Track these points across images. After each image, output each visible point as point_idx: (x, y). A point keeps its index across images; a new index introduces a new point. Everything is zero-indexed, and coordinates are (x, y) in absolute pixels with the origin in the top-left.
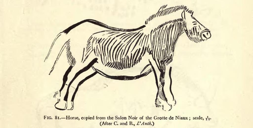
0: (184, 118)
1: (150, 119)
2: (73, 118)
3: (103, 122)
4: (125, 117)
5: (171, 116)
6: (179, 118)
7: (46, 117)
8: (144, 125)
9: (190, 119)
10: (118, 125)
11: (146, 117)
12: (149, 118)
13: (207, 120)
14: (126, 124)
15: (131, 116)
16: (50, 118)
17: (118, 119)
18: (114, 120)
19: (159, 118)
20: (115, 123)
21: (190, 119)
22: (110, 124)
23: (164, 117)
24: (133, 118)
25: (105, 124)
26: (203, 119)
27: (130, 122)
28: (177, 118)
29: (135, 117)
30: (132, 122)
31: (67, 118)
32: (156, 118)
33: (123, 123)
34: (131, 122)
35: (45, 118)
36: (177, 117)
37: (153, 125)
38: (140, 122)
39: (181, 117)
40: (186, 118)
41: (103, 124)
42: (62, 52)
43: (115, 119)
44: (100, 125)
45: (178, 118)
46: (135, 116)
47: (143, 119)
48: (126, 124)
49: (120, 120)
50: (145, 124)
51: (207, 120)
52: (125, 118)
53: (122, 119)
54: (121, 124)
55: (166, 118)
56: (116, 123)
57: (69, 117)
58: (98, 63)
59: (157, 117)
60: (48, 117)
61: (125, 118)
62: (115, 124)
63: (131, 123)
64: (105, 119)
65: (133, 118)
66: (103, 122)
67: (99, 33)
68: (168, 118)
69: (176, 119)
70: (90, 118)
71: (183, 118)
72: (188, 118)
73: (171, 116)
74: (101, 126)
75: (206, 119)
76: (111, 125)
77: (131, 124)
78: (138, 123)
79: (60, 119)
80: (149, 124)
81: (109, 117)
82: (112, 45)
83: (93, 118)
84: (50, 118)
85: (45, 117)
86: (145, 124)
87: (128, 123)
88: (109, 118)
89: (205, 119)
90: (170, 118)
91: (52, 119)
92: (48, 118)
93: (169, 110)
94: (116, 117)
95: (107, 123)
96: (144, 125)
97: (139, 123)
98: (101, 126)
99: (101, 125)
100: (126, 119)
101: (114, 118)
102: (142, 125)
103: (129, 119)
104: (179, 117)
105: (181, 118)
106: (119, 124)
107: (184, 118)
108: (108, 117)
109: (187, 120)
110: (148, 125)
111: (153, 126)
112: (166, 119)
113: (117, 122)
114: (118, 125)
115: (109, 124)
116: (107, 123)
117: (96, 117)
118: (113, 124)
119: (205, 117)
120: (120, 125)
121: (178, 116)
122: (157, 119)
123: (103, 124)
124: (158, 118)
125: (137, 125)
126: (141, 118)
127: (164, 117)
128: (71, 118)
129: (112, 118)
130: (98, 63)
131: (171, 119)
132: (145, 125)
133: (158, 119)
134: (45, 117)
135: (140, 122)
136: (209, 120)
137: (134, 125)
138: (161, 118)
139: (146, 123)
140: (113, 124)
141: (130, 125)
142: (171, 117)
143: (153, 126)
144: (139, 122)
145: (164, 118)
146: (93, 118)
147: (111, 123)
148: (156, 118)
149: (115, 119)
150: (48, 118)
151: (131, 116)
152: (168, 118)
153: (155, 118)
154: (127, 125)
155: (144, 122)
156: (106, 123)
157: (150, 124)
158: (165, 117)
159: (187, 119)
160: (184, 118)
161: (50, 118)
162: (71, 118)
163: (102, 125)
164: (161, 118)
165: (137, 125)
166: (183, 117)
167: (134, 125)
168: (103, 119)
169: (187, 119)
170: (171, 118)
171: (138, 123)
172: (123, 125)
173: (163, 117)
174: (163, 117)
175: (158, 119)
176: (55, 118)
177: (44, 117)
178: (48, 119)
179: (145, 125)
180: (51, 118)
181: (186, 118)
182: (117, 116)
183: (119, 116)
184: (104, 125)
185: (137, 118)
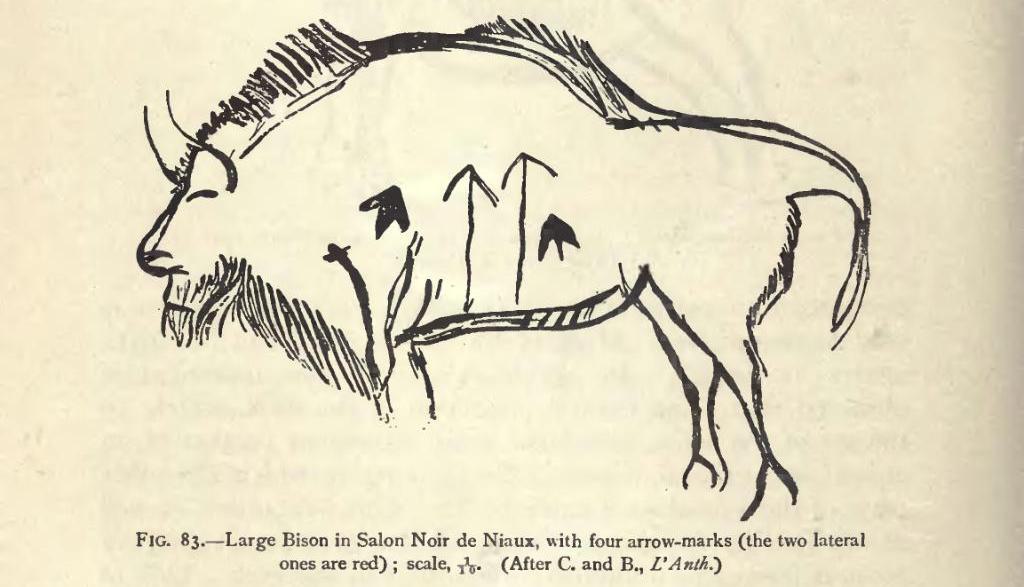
0: (519, 543)
2: (846, 539)
3: (516, 558)
4: (321, 539)
5: (465, 534)
6: (498, 542)
7: (144, 539)
9: (395, 569)
10: (573, 569)
12: (758, 541)
13: (355, 568)
14: (607, 566)
15: (424, 534)
16: (160, 541)
17: (370, 545)
18: (624, 550)
20: (564, 561)
21: (395, 569)
22: (544, 566)
24: (432, 542)
25: (523, 566)
26: (449, 569)
28: (417, 542)
29: (436, 537)
33: (595, 563)
34: (628, 561)
35: (142, 542)
36: (492, 540)
43: (359, 545)
45: (423, 543)
46: (439, 534)
48: (607, 566)
49: (706, 547)
50: (682, 566)
51: (355, 568)
52: (701, 543)
53: (429, 545)
54: (586, 566)
56: (565, 563)
58: (349, 247)
60: (152, 537)
62: (564, 567)
63: (627, 564)
64: (326, 545)
65: (432, 542)
66: (516, 558)
69: (414, 545)
70: (790, 542)
73: (465, 534)
75: (461, 567)
76: (547, 569)
77: (628, 567)
79: (203, 545)
82: (620, 277)
85: (142, 536)
86: (682, 566)
87: (617, 564)
89: (455, 570)
90: (462, 542)
91: (168, 545)
94: (363, 536)
95: (532, 562)
96: (678, 569)
97: (660, 563)
101: (355, 540)
102: (671, 569)
103: (486, 545)
104: (498, 537)
106: (579, 566)
107: (516, 542)
109: (529, 548)
110: (696, 569)
111: (716, 573)
114: (573, 569)
116: (529, 560)
117: (592, 539)
118: (554, 566)
121: (495, 534)
123: (514, 564)
125: (653, 569)
129: (765, 541)
130: (349, 247)
136: (472, 571)
137: (642, 570)
138: (656, 543)
139: (687, 564)
140: (554, 566)
141: (624, 569)
143: (716, 573)
145: (831, 542)
149: (359, 545)
151: (424, 534)
154: (611, 569)
156: (526, 562)
157: (703, 564)
160: (516, 542)
161: (160, 541)
163: (512, 569)
165: (653, 569)
172: (595, 569)
177: (139, 539)
178: (152, 545)
180: (164, 542)
181: (525, 542)
182: (366, 534)
183: (373, 534)
184: (520, 569)
185: (445, 540)
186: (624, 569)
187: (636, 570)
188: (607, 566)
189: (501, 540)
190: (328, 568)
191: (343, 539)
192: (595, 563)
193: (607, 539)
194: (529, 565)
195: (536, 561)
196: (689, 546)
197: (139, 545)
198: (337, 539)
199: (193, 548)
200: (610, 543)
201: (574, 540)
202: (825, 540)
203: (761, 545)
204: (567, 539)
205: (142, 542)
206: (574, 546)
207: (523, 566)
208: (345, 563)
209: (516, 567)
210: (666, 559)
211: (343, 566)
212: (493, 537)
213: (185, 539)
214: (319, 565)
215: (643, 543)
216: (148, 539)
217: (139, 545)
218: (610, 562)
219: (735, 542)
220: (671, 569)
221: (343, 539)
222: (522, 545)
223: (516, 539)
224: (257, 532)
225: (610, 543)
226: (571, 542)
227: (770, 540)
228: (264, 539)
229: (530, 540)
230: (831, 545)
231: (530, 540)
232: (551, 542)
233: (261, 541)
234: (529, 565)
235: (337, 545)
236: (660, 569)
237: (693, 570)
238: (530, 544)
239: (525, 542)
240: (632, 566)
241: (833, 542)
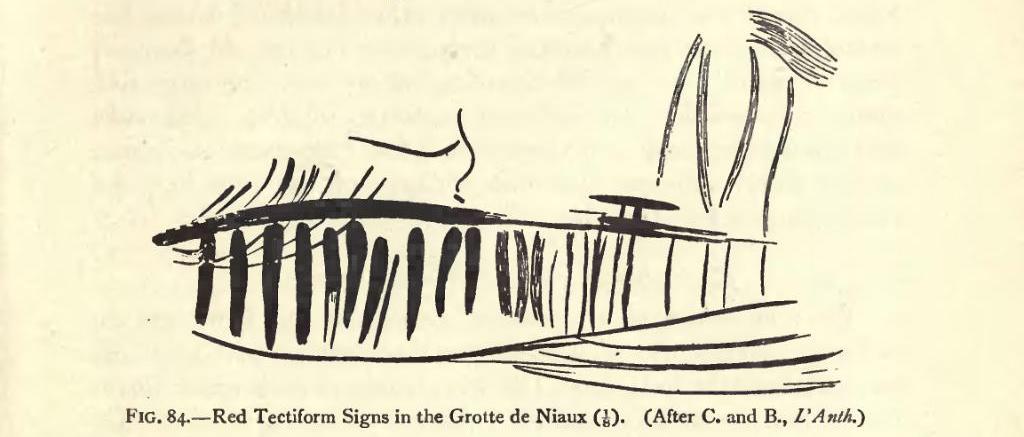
1: (524, 421)
3: (660, 411)
8: (822, 421)
10: (718, 421)
12: (429, 417)
14: (752, 418)
19: (470, 418)
20: (708, 413)
22: (687, 419)
23: (492, 415)
25: (666, 419)
27: (768, 411)
28: (542, 418)
30: (775, 412)
32: (461, 418)
33: (738, 416)
34: (771, 413)
36: (543, 413)
37: (859, 422)
39: (557, 413)
40: (580, 415)
42: (492, 361)
43: (344, 421)
45: (547, 419)
46: (397, 411)
50: (826, 418)
55: (498, 417)
56: (709, 416)
59: (463, 414)
60: (141, 414)
63: (771, 416)
66: (660, 411)
67: (354, 362)
68: (507, 418)
69: (539, 421)
71: (566, 418)
72: (585, 418)
74: (651, 426)
76: (690, 421)
77: (771, 419)
78: (799, 415)
79: (189, 421)
81: (423, 413)
84: (150, 419)
85: (132, 412)
86: (826, 418)
87: (761, 416)
88: (423, 418)
90: (515, 418)
92: (143, 418)
93: (837, 385)
96: (822, 421)
98: (651, 426)
99: (650, 421)
100: (333, 421)
102: (814, 421)
103: (539, 421)
104: (552, 412)
106: (724, 419)
108: (419, 415)
109: (582, 424)
110: (839, 421)
112: (500, 420)
113: (713, 411)
114: (718, 421)
115: (683, 419)
116: (672, 413)
118: (698, 419)
120: (729, 421)
121: (548, 410)
122: (464, 419)
123: (657, 417)
125: (797, 420)
127: (492, 415)
128: (308, 419)
131: (518, 421)
132: (829, 421)
133: (467, 421)
134: (129, 415)
135: (810, 411)
137: (785, 422)
138: (477, 419)
139: (831, 416)
140: (698, 419)
141: (767, 421)
142: (518, 414)
144: (805, 412)
147: (690, 416)
148: (461, 418)
149: (344, 421)
150: (143, 418)
152: (507, 418)
153: (456, 418)
155: (823, 411)
156: (669, 415)
159: (585, 422)
161: (150, 417)
162: (308, 419)
163: (655, 421)
164: (477, 419)
165: (797, 420)
167: (782, 423)
168: (326, 420)
169: (585, 422)
170: (519, 417)
171: (799, 415)
173: (485, 415)
174: (488, 413)
175: (467, 421)
176: (168, 419)
178: (141, 421)
179: (829, 421)
180: (154, 419)
184: (664, 421)
187: (779, 421)
188: (752, 418)
189: (554, 416)
190: (734, 421)
191: (403, 416)
192: (738, 416)
193: (744, 422)
196: (328, 422)
197: (129, 421)
198: (397, 416)
199: (266, 410)
201: (427, 415)
202: (564, 416)
203: (432, 422)
205: (131, 418)
206: (328, 422)
207: (666, 419)
208: (441, 416)
209: (659, 420)
210: (810, 411)
211: (439, 419)
213: (171, 415)
215: (319, 419)
216: (138, 416)
217: (129, 421)
218: (754, 414)
219: (589, 418)
221: (403, 416)
222: (575, 421)
223: (569, 415)
225: (741, 418)
227: (528, 416)
228: (368, 416)
230: (223, 421)
233: (365, 418)
235: (397, 421)
236: (804, 421)
237: (836, 423)
240: (775, 418)
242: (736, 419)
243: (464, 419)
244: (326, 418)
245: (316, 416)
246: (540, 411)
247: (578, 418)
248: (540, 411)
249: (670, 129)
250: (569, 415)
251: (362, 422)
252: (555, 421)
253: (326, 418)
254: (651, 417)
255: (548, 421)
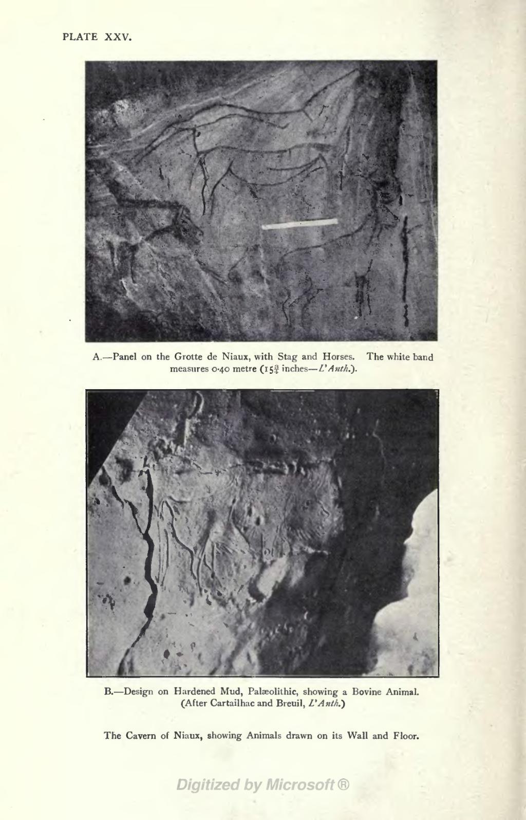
3: (189, 700)
4: (324, 735)
5: (290, 732)
11: (158, 356)
14: (269, 704)
19: (185, 357)
25: (192, 704)
28: (225, 357)
31: (328, 355)
32: (180, 357)
37: (342, 706)
38: (316, 701)
41: (189, 705)
44: (182, 704)
45: (180, 737)
47: (167, 738)
50: (325, 704)
55: (199, 357)
56: (214, 703)
57: (180, 691)
59: (182, 355)
61: (149, 357)
62: (214, 704)
64: (151, 359)
66: (189, 700)
71: (238, 358)
73: (290, 732)
80: (334, 704)
83: (213, 692)
84: (178, 358)
87: (275, 703)
88: (159, 357)
90: (210, 357)
94: (281, 354)
97: (314, 703)
99: (184, 705)
102: (319, 706)
105: (233, 358)
110: (332, 706)
118: (208, 704)
119: (236, 602)
122: (182, 358)
124: (184, 356)
126: (163, 737)
127: (196, 355)
128: (334, 357)
135: (316, 701)
140: (208, 704)
141: (278, 706)
146: (213, 692)
148: (180, 357)
153: (178, 358)
155: (323, 701)
156: (194, 702)
158: (198, 355)
162: (334, 357)
163: (186, 705)
164: (189, 357)
166: (210, 790)
177: (395, 736)
186: (278, 706)
191: (286, 368)
194: (195, 703)
195: (199, 702)
197: (395, 738)
198: (334, 735)
200: (294, 704)
204: (281, 690)
207: (192, 704)
210: (326, 365)
212: (227, 354)
214: (256, 704)
215: (150, 737)
216: (400, 735)
217: (250, 694)
220: (319, 706)
223: (239, 356)
224: (277, 793)
226: (283, 692)
228: (147, 691)
229: (246, 356)
230: (196, 359)
231: (246, 356)
232: (257, 357)
234: (195, 703)
238: (246, 358)
239: (244, 357)
241: (197, 357)
242: (236, 369)
243: (182, 358)
244: (265, 736)
245: (338, 356)
246: (176, 733)
247: (195, 736)
248: (176, 733)
249: (402, 237)
250: (239, 356)
251: (293, 359)
252: (183, 738)
253: (265, 736)
254: (184, 703)
255: (228, 358)
